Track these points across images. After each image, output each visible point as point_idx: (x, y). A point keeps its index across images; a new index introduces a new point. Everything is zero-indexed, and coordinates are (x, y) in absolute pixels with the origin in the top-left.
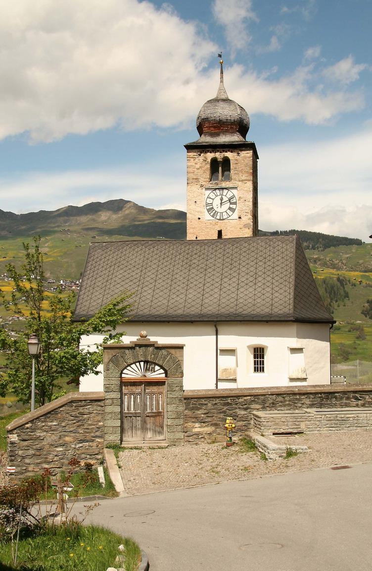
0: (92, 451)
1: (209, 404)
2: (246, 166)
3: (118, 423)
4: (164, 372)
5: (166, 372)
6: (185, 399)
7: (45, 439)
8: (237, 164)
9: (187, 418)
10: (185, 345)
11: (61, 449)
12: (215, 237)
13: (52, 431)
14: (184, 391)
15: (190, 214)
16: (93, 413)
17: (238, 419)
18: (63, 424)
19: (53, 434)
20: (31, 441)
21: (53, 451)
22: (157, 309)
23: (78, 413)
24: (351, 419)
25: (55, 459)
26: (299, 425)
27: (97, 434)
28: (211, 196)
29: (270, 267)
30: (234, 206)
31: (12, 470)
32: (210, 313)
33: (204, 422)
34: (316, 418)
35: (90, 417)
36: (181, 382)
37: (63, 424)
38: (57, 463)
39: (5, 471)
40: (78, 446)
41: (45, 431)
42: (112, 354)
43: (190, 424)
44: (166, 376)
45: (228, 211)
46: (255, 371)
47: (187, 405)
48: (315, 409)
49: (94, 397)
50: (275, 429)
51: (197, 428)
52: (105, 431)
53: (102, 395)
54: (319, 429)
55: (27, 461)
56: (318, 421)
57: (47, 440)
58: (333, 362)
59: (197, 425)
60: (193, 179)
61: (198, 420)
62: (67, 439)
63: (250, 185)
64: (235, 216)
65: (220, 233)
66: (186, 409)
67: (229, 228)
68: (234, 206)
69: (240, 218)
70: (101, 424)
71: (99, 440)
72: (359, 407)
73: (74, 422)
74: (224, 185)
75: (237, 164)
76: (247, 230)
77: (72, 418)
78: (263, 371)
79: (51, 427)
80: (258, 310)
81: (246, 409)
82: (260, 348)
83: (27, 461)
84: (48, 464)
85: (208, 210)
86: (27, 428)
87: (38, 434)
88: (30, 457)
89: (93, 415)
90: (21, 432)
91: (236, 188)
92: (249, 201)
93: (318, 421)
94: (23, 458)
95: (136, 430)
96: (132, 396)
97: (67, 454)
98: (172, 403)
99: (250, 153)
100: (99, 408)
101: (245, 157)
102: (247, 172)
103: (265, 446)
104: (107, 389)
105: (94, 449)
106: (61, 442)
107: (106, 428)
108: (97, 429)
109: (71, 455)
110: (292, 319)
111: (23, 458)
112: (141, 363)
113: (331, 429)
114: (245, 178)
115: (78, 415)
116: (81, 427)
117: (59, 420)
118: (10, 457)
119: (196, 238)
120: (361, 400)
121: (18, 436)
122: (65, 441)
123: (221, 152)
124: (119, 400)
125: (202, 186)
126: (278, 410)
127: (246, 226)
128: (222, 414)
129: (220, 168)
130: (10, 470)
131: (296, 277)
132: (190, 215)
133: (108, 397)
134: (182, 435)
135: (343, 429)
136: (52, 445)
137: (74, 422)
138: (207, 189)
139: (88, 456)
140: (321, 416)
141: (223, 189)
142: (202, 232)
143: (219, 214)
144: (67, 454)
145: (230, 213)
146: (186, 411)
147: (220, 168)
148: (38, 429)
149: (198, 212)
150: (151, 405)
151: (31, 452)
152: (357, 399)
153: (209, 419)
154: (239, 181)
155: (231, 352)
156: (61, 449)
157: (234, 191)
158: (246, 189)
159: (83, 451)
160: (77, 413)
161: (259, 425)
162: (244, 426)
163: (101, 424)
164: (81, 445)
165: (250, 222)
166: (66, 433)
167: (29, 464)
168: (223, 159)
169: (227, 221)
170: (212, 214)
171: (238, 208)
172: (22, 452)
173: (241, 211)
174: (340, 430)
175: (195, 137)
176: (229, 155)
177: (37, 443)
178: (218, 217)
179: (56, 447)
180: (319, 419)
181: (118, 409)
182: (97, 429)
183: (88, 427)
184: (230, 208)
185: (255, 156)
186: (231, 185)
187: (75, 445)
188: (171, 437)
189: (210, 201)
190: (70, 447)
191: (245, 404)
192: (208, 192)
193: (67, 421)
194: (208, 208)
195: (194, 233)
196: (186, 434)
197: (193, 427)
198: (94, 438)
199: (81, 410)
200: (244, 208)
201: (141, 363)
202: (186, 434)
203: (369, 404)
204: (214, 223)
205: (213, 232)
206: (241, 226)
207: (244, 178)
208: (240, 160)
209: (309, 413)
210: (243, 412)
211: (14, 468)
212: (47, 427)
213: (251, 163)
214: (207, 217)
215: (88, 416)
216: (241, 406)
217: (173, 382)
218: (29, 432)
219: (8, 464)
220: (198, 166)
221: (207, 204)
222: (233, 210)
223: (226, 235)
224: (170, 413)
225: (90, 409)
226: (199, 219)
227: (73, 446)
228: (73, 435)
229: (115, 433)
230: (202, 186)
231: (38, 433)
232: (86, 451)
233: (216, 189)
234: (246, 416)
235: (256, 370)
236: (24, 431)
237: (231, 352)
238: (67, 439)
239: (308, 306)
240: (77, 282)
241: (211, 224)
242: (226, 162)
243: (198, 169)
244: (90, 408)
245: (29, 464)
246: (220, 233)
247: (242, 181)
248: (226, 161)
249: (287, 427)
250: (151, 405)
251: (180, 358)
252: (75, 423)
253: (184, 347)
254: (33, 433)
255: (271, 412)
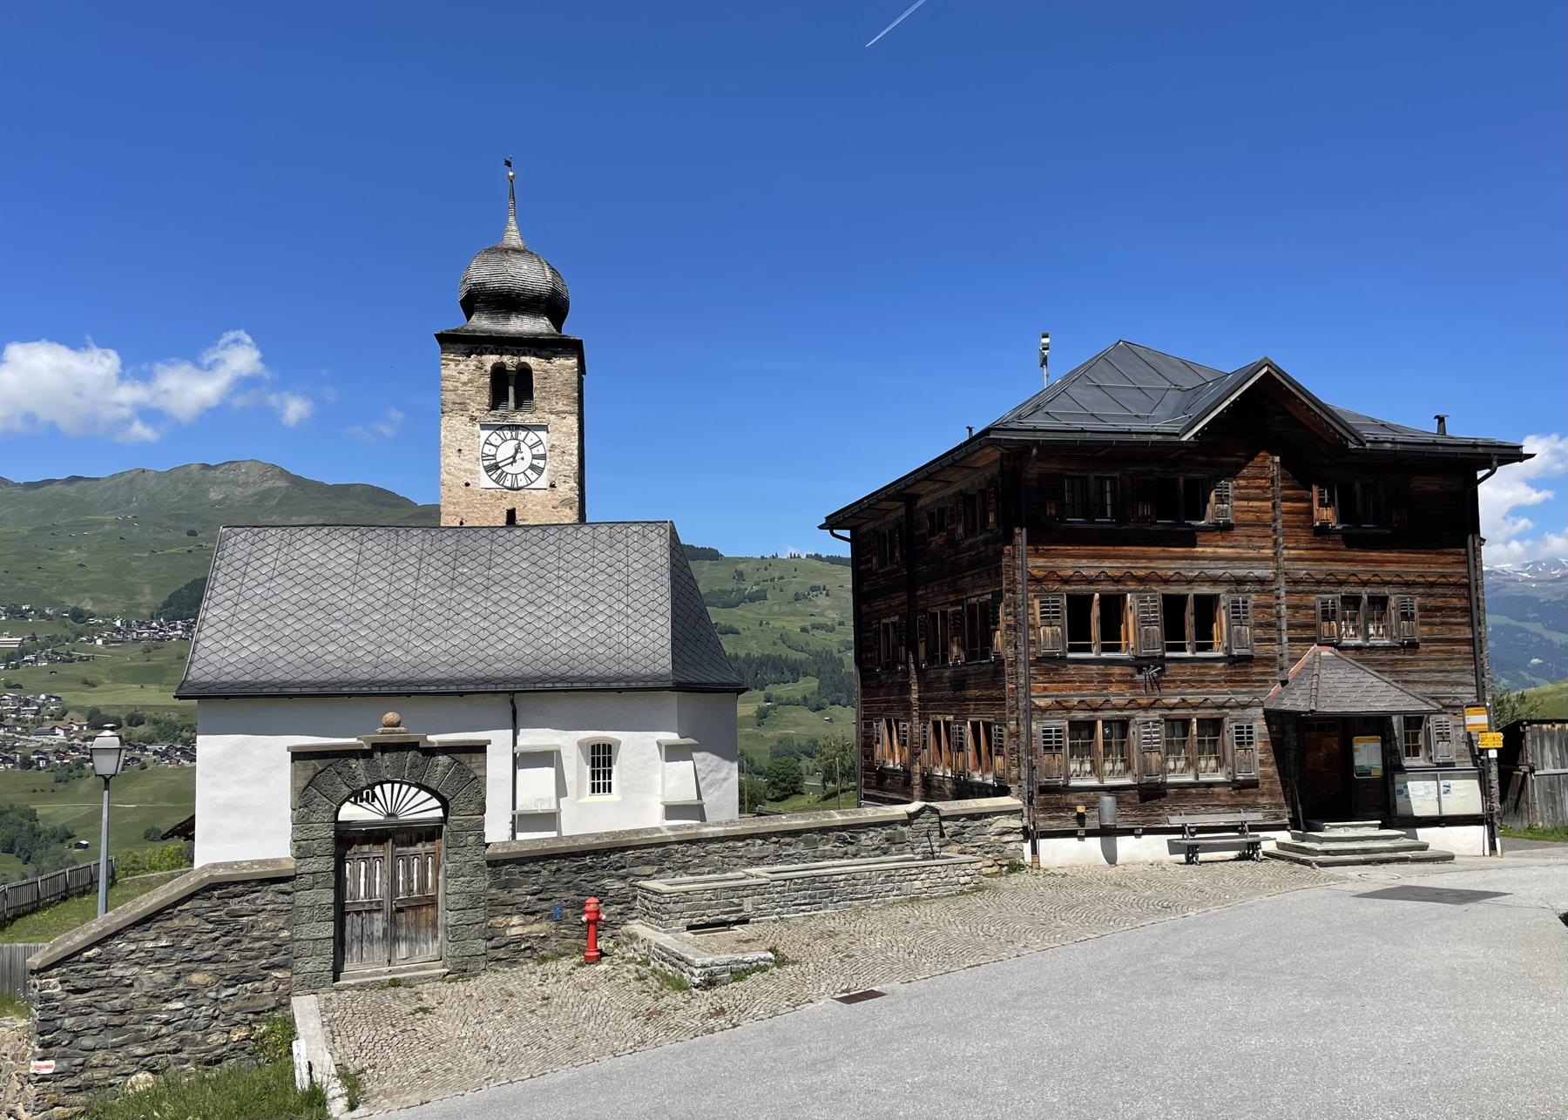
0: (261, 1003)
1: (544, 873)
2: (564, 385)
3: (328, 930)
4: (439, 804)
5: (445, 805)
6: (489, 863)
7: (136, 984)
8: (546, 378)
9: (496, 907)
10: (489, 742)
11: (180, 1005)
12: (502, 521)
13: (157, 961)
14: (487, 845)
15: (448, 473)
16: (264, 910)
17: (607, 900)
18: (187, 943)
19: (159, 968)
20: (100, 992)
21: (159, 1011)
22: (382, 668)
23: (227, 914)
24: (842, 884)
25: (164, 1031)
26: (741, 905)
27: (274, 959)
28: (492, 439)
29: (404, 630)
30: (541, 463)
31: (48, 1067)
32: (501, 675)
33: (532, 914)
34: (774, 886)
35: (257, 921)
36: (481, 825)
37: (187, 943)
38: (168, 1039)
39: (24, 1072)
40: (224, 994)
41: (137, 963)
42: (315, 768)
43: (500, 919)
44: (446, 811)
45: (529, 472)
46: (593, 791)
47: (495, 875)
48: (766, 868)
49: (270, 871)
50: (692, 917)
51: (516, 926)
52: (295, 950)
53: (290, 866)
54: (779, 910)
55: (87, 1042)
56: (778, 893)
57: (142, 985)
58: (293, 761)
59: (516, 920)
60: (454, 403)
61: (518, 908)
62: (196, 978)
63: (572, 421)
64: (543, 482)
65: (511, 515)
66: (490, 886)
67: (530, 505)
68: (541, 463)
69: (552, 486)
70: (285, 934)
71: (279, 975)
72: (849, 858)
73: (216, 934)
74: (519, 418)
75: (546, 378)
76: (567, 511)
77: (211, 926)
78: (610, 791)
79: (151, 952)
80: (601, 668)
81: (624, 878)
82: (604, 745)
83: (87, 1042)
84: (144, 1046)
85: (488, 469)
86: (89, 960)
87: (120, 973)
88: (95, 1031)
89: (263, 916)
90: (72, 970)
91: (544, 428)
92: (571, 455)
93: (778, 893)
94: (76, 1035)
95: (371, 942)
96: (363, 864)
97: (195, 1015)
98: (460, 874)
99: (573, 361)
100: (281, 898)
101: (565, 368)
102: (568, 397)
103: (681, 959)
104: (302, 852)
105: (265, 996)
106: (180, 986)
107: (297, 944)
108: (275, 949)
109: (205, 1016)
110: (669, 684)
111: (76, 1035)
112: (385, 786)
113: (803, 907)
114: (564, 408)
115: (226, 918)
116: (235, 946)
117: (176, 933)
118: (38, 1036)
119: (461, 523)
120: (852, 844)
121: (61, 982)
122: (188, 983)
123: (513, 354)
124: (332, 876)
125: (473, 419)
126: (692, 874)
127: (565, 503)
128: (573, 892)
129: (511, 390)
130: (40, 1067)
131: (673, 604)
132: (449, 477)
133: (304, 869)
134: (481, 945)
135: (826, 907)
136: (157, 997)
137: (216, 934)
138: (484, 427)
139: (251, 1016)
140: (782, 883)
141: (517, 427)
142: (473, 512)
143: (509, 477)
144: (195, 1015)
145: (533, 476)
146: (493, 891)
147: (511, 390)
148: (118, 959)
149: (465, 471)
150: (409, 880)
151: (98, 1019)
152: (845, 841)
153: (545, 905)
154: (552, 413)
155: (546, 758)
156: (180, 1005)
157: (542, 434)
158: (564, 429)
159: (238, 1003)
160: (222, 913)
161: (657, 910)
162: (619, 914)
163: (285, 934)
164: (231, 991)
165: (574, 495)
166: (195, 965)
167: (93, 1050)
168: (517, 367)
169: (527, 491)
170: (494, 477)
171: (548, 466)
172: (72, 1020)
173: (556, 472)
174: (821, 909)
175: (456, 321)
176: (531, 361)
177: (115, 995)
178: (508, 484)
179: (167, 1001)
180: (779, 889)
181: (328, 897)
182: (275, 949)
183: (250, 946)
184: (532, 467)
185: (582, 369)
186: (535, 421)
187: (217, 991)
188: (457, 953)
189: (489, 450)
190: (205, 997)
191: (623, 867)
192: (485, 434)
193: (195, 936)
194: (486, 463)
195: (456, 514)
196: (490, 944)
197: (507, 926)
198: (265, 972)
199: (234, 905)
200: (561, 468)
201: (385, 786)
202: (490, 944)
203: (868, 851)
204: (499, 495)
205: (497, 512)
206: (555, 503)
207: (560, 407)
208: (552, 373)
209: (758, 877)
210: (618, 885)
211: (52, 1062)
212: (143, 954)
213: (575, 378)
214: (486, 481)
215: (251, 918)
216: (614, 872)
217: (461, 825)
218: (93, 968)
219: (34, 1053)
220: (464, 378)
221: (485, 457)
222: (539, 471)
223: (524, 520)
224: (453, 898)
225: (258, 901)
226: (467, 485)
227: (212, 995)
228: (213, 967)
229: (321, 955)
230: (473, 419)
231: (117, 971)
232: (246, 1003)
233: (501, 428)
234: (623, 892)
235: (595, 789)
236: (80, 967)
237: (546, 758)
238: (196, 978)
239: (697, 659)
240: (154, 624)
241: (492, 495)
242: (524, 378)
243: (465, 384)
244: (257, 898)
245: (93, 1050)
246: (511, 515)
247: (557, 413)
248: (525, 373)
249: (717, 911)
250: (409, 880)
251: (478, 773)
252: (216, 939)
253: (488, 746)
254: (105, 972)
255: (678, 879)
